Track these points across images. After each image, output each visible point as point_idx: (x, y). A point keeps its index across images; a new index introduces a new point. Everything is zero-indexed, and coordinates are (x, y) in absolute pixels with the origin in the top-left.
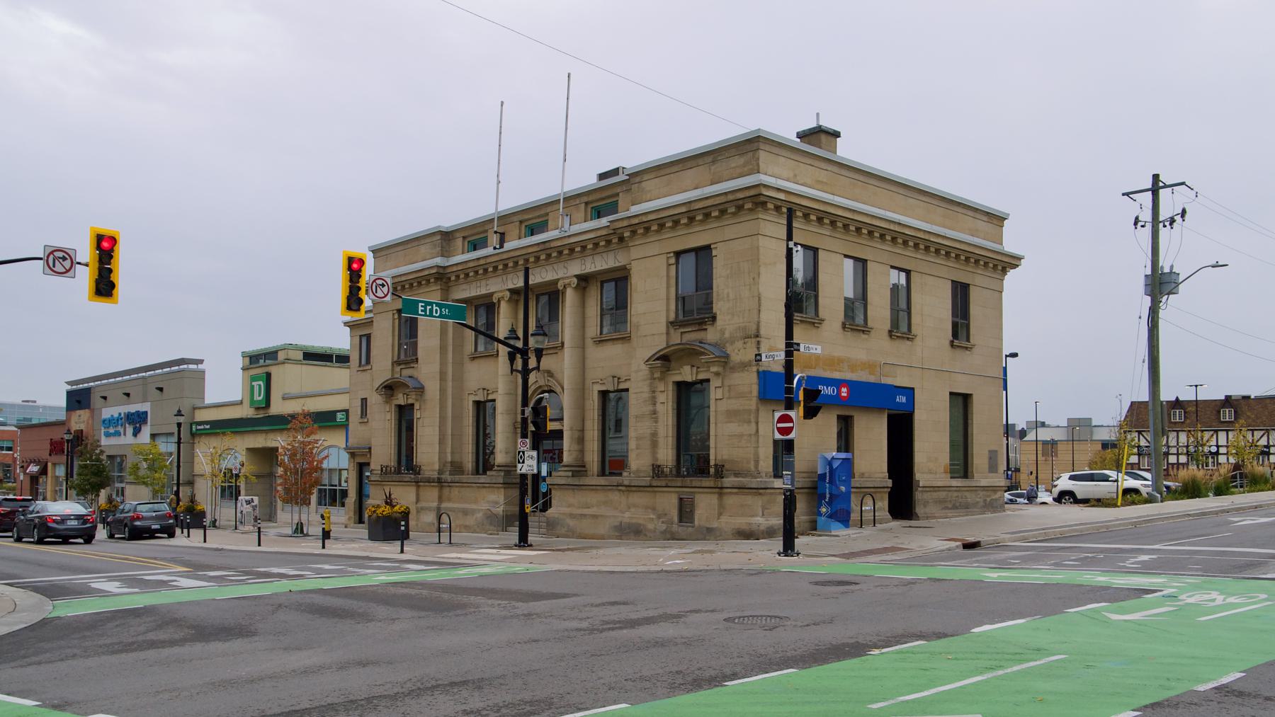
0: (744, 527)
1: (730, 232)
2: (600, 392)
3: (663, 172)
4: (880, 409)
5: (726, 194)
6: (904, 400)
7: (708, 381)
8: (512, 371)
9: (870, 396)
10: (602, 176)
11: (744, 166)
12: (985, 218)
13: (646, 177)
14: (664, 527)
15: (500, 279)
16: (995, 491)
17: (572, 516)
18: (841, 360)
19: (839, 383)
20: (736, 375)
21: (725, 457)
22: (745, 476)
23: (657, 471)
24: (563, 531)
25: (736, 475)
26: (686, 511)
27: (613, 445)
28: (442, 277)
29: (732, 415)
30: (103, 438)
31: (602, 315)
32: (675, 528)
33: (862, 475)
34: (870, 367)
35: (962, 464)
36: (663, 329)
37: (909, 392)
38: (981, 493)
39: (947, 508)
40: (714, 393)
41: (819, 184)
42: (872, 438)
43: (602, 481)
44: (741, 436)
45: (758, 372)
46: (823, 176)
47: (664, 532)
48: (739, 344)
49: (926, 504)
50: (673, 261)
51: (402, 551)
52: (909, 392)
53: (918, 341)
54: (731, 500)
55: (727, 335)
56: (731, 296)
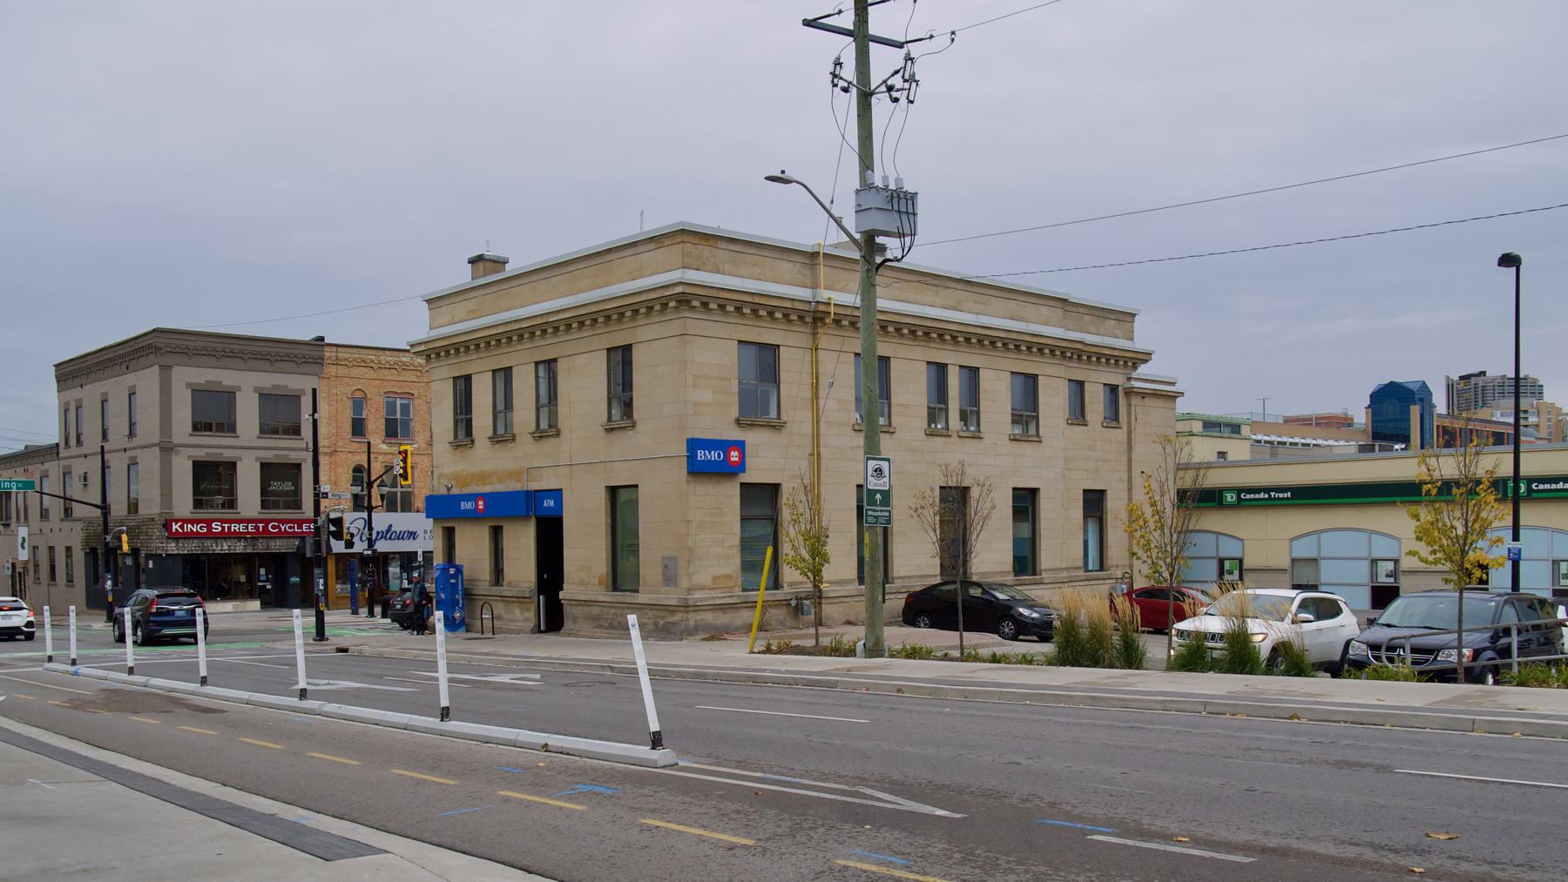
4: (527, 517)
6: (552, 503)
9: (499, 510)
12: (652, 246)
16: (673, 613)
18: (490, 474)
19: (474, 497)
27: (1025, 530)
30: (355, 550)
31: (538, 410)
33: (510, 584)
34: (516, 474)
35: (621, 574)
37: (557, 494)
38: (650, 613)
39: (601, 627)
41: (473, 314)
42: (522, 544)
46: (471, 305)
49: (575, 619)
52: (557, 494)
53: (565, 434)
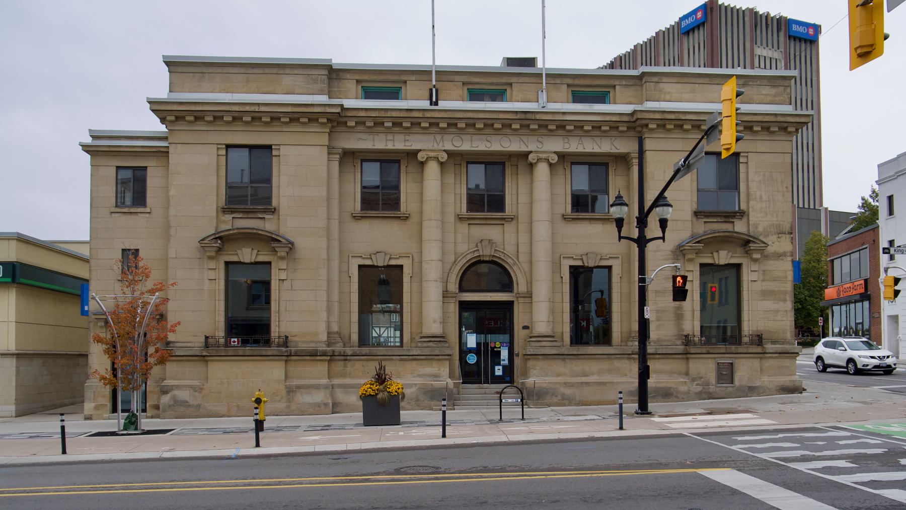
0: (788, 384)
1: (762, 146)
2: (571, 267)
3: (685, 80)
5: (776, 115)
7: (269, 263)
8: (620, 238)
10: (511, 62)
11: (776, 95)
13: (665, 79)
14: (700, 389)
15: (431, 137)
17: (566, 384)
20: (771, 262)
21: (762, 328)
22: (783, 343)
23: (687, 340)
24: (555, 400)
25: (774, 342)
26: (726, 374)
28: (337, 120)
29: (766, 294)
32: (712, 388)
36: (215, 214)
40: (747, 276)
43: (575, 350)
44: (777, 311)
45: (793, 261)
47: (700, 393)
48: (773, 238)
50: (223, 152)
51: (444, 436)
54: (769, 363)
55: (760, 229)
56: (765, 198)
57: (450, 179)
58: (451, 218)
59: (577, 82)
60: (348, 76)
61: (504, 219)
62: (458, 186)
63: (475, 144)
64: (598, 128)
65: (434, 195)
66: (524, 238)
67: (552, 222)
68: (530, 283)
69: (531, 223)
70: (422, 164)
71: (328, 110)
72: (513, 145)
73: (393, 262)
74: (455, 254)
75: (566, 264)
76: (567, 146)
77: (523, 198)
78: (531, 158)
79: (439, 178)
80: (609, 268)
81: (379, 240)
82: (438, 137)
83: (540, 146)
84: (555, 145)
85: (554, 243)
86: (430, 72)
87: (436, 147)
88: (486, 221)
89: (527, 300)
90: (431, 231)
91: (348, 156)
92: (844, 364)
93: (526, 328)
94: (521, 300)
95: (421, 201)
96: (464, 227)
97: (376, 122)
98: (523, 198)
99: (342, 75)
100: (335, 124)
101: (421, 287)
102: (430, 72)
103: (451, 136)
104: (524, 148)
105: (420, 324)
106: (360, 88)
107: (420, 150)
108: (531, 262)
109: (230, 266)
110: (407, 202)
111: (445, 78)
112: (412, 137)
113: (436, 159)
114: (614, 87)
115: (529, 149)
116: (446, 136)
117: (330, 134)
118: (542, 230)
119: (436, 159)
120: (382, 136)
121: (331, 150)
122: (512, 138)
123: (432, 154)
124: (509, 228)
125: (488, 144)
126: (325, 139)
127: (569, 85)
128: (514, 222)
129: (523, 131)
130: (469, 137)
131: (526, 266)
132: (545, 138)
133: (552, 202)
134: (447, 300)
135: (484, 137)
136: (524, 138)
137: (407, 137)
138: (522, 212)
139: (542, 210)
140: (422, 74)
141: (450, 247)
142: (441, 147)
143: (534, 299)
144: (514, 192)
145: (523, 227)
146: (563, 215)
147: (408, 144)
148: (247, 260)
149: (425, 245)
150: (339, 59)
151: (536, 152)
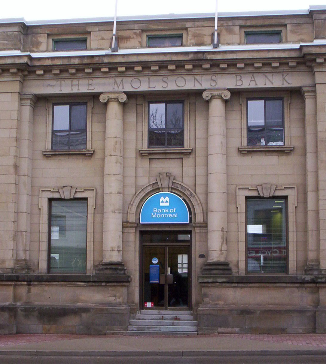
15: (112, 81)
57: (132, 118)
58: (131, 154)
59: (249, 23)
60: (39, 30)
61: (183, 153)
62: (139, 124)
63: (152, 85)
64: (267, 64)
65: (117, 133)
66: (200, 171)
67: (227, 155)
68: (205, 214)
69: (207, 156)
70: (208, 102)
71: (17, 61)
72: (188, 84)
73: (79, 195)
74: (136, 186)
75: (242, 195)
76: (239, 83)
77: (200, 133)
78: (205, 95)
79: (224, 115)
80: (286, 198)
81: (66, 174)
82: (119, 80)
83: (213, 84)
84: (228, 82)
85: (228, 175)
86: (213, 19)
87: (116, 89)
88: (166, 156)
89: (203, 230)
90: (112, 166)
91: (42, 102)
92: (11, 271)
93: (201, 256)
94: (197, 230)
95: (104, 139)
96: (144, 164)
97: (63, 70)
98: (200, 133)
99: (35, 30)
100: (26, 73)
101: (102, 218)
102: (213, 19)
103: (130, 79)
104: (198, 87)
105: (102, 251)
106: (51, 41)
107: (102, 93)
108: (207, 193)
109: (53, 203)
110: (92, 141)
111: (125, 27)
112: (95, 81)
113: (220, 97)
114: (285, 25)
115: (203, 88)
116: (125, 79)
117: (22, 83)
118: (217, 164)
119: (220, 97)
120: (68, 82)
121: (22, 97)
122: (187, 78)
123: (113, 96)
124: (188, 161)
125: (165, 85)
126: (16, 87)
127: (241, 27)
128: (192, 156)
129: (196, 71)
130: (146, 79)
131: (202, 197)
132: (219, 76)
133: (227, 136)
134: (126, 230)
135: (161, 78)
136: (269, 76)
137: (91, 82)
138: (200, 145)
139: (216, 143)
140: (107, 25)
141: (130, 181)
142: (120, 89)
143: (209, 228)
144: (192, 128)
145: (200, 160)
146: (239, 148)
147: (91, 88)
148: (67, 197)
149: (106, 178)
150: (31, 17)
151: (210, 90)
